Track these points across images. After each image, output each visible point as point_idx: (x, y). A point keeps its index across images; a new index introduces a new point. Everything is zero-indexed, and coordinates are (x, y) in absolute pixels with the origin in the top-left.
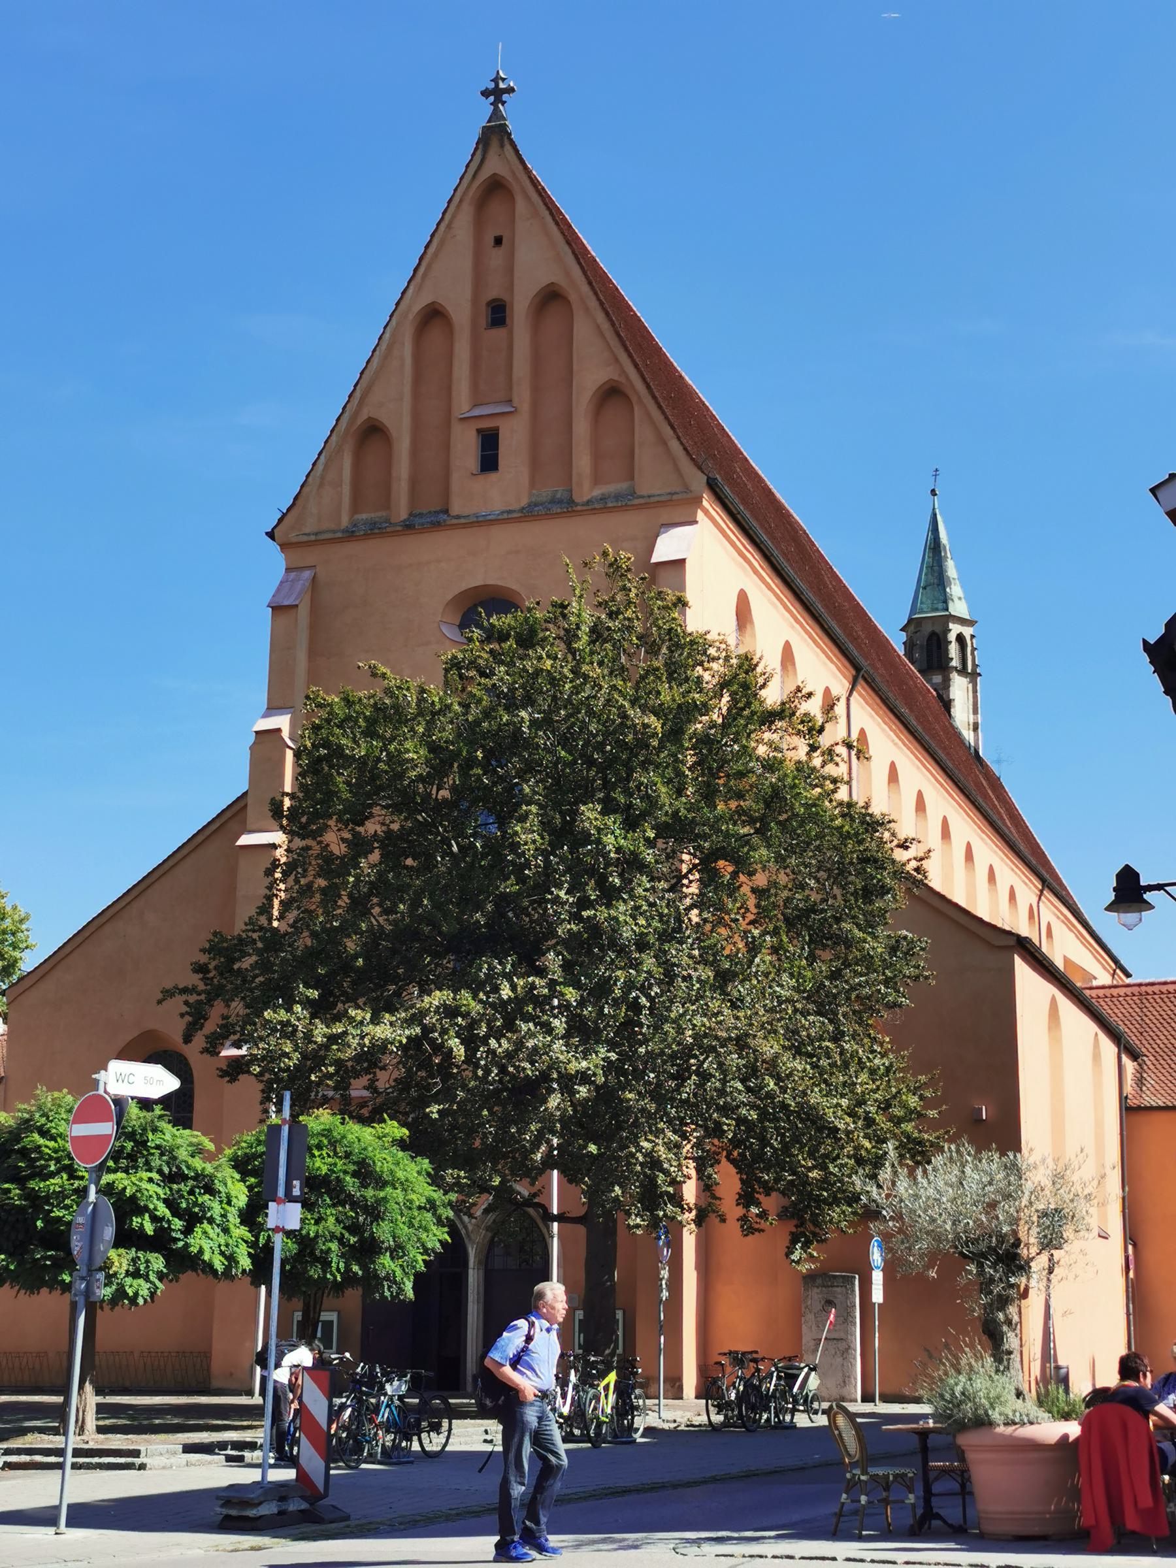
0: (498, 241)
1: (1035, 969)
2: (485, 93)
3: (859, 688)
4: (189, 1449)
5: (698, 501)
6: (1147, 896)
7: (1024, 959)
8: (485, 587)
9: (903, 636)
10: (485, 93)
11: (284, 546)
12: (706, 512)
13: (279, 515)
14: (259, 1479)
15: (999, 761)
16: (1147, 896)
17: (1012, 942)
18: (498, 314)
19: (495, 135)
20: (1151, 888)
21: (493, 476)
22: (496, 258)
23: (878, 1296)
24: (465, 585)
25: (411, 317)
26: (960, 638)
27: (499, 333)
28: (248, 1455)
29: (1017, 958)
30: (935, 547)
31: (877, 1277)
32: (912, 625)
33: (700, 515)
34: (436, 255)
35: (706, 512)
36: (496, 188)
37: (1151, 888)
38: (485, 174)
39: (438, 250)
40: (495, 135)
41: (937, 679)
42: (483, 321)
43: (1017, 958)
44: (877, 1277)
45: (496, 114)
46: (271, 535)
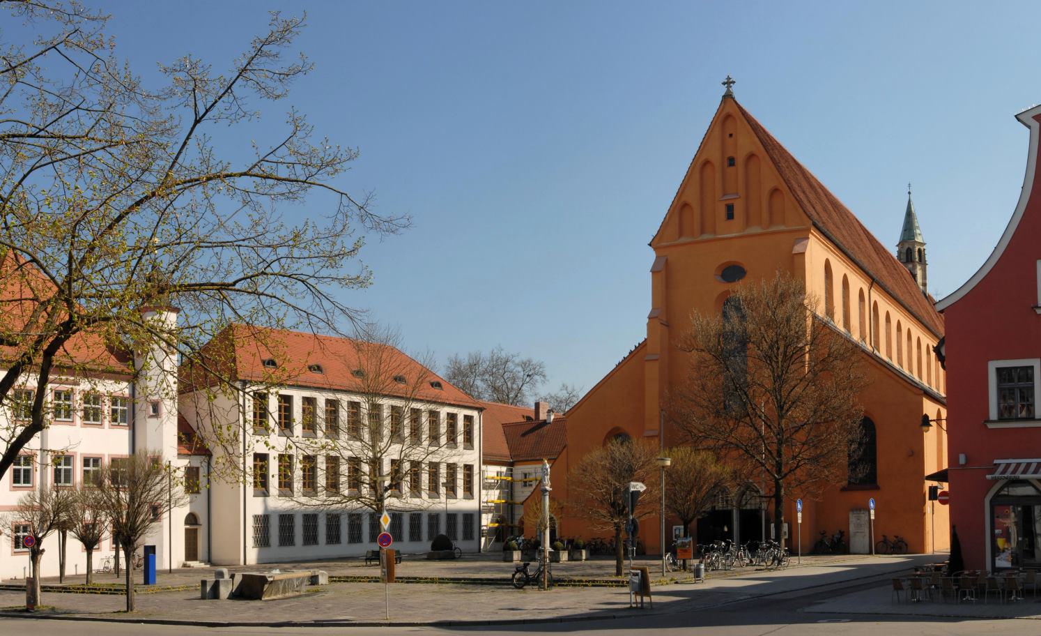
0: (731, 135)
1: (931, 401)
2: (724, 84)
3: (874, 285)
4: (25, 568)
5: (808, 231)
6: (931, 423)
7: (927, 398)
8: (728, 262)
9: (897, 249)
10: (724, 84)
11: (655, 249)
12: (813, 234)
13: (653, 237)
14: (123, 450)
15: (937, 295)
16: (931, 423)
17: (922, 392)
18: (732, 161)
19: (728, 97)
20: (931, 421)
21: (731, 221)
22: (729, 141)
23: (873, 517)
24: (724, 260)
25: (699, 164)
26: (919, 250)
27: (732, 168)
28: (337, 579)
29: (924, 399)
30: (909, 215)
31: (872, 512)
32: (901, 244)
33: (810, 235)
34: (706, 142)
35: (813, 234)
36: (728, 116)
37: (931, 421)
38: (724, 113)
39: (708, 138)
40: (728, 97)
41: (910, 266)
42: (726, 164)
43: (924, 399)
44: (872, 512)
45: (728, 90)
46: (650, 245)
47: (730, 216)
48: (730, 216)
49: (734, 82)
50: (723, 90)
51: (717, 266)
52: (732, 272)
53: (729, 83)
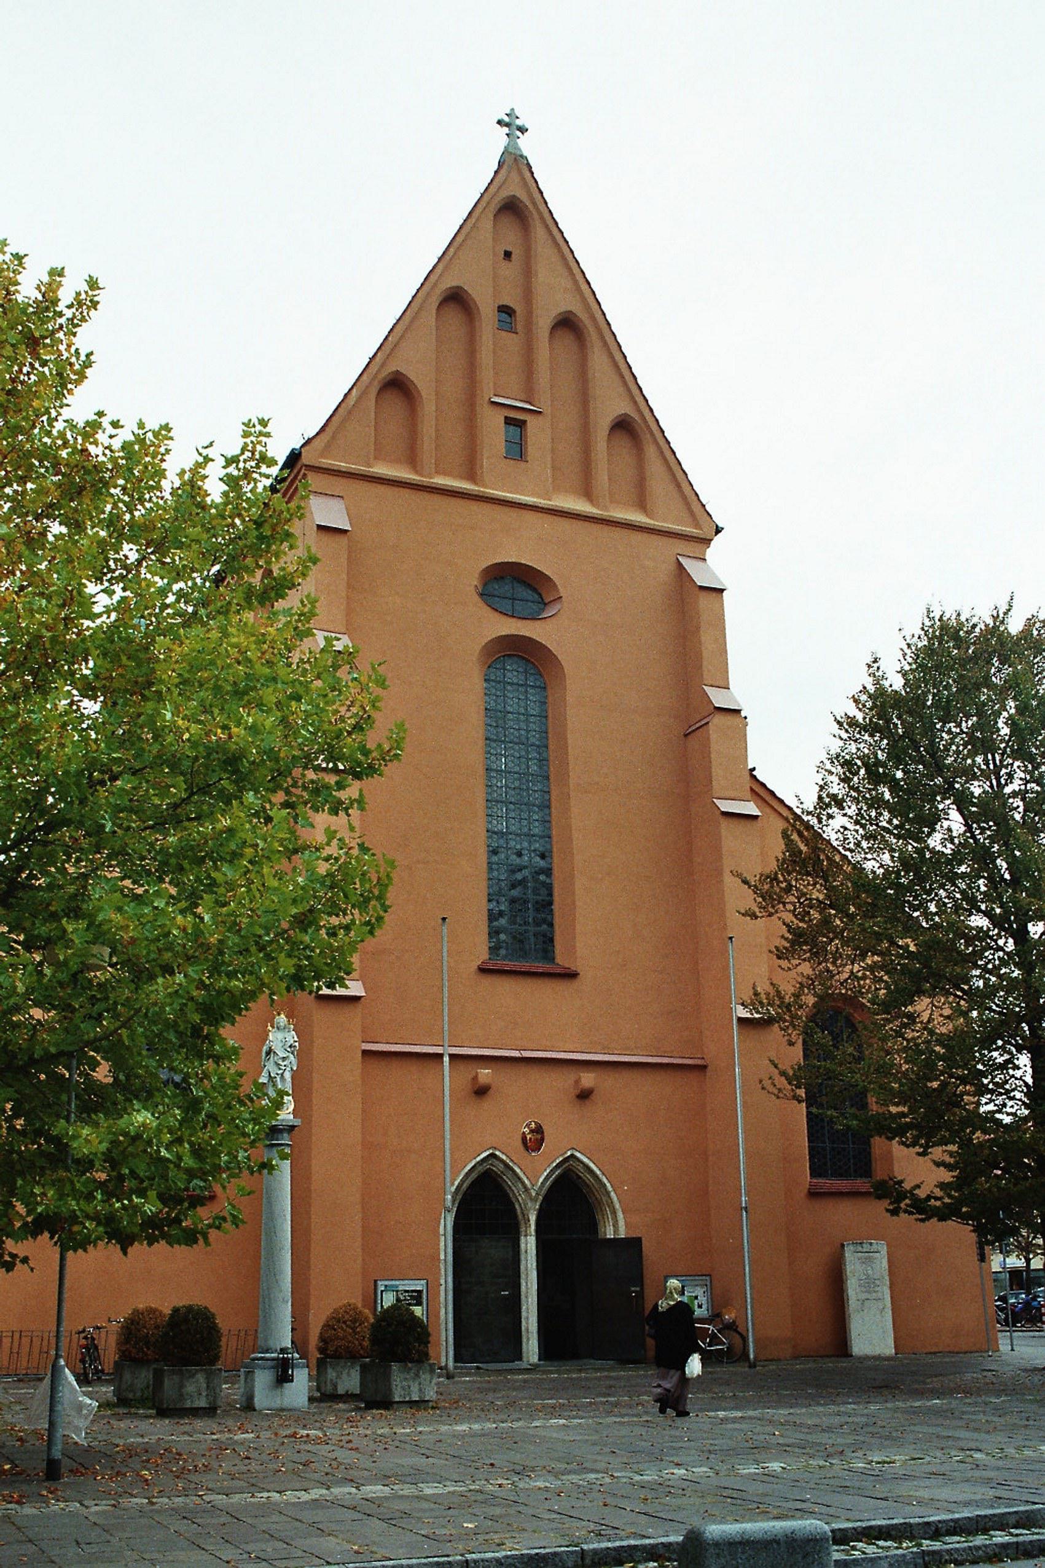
0: (508, 255)
19: (514, 164)
40: (514, 164)
47: (518, 451)
48: (518, 451)
49: (523, 130)
50: (499, 139)
51: (485, 564)
52: (515, 585)
53: (511, 125)
